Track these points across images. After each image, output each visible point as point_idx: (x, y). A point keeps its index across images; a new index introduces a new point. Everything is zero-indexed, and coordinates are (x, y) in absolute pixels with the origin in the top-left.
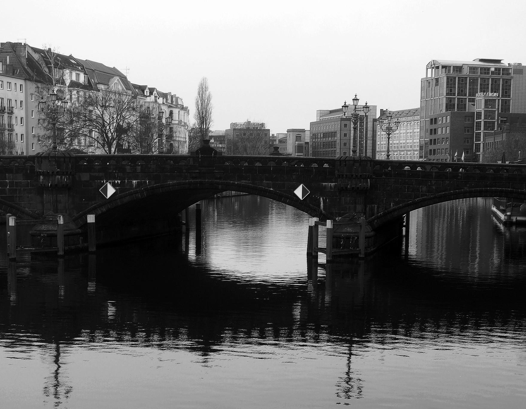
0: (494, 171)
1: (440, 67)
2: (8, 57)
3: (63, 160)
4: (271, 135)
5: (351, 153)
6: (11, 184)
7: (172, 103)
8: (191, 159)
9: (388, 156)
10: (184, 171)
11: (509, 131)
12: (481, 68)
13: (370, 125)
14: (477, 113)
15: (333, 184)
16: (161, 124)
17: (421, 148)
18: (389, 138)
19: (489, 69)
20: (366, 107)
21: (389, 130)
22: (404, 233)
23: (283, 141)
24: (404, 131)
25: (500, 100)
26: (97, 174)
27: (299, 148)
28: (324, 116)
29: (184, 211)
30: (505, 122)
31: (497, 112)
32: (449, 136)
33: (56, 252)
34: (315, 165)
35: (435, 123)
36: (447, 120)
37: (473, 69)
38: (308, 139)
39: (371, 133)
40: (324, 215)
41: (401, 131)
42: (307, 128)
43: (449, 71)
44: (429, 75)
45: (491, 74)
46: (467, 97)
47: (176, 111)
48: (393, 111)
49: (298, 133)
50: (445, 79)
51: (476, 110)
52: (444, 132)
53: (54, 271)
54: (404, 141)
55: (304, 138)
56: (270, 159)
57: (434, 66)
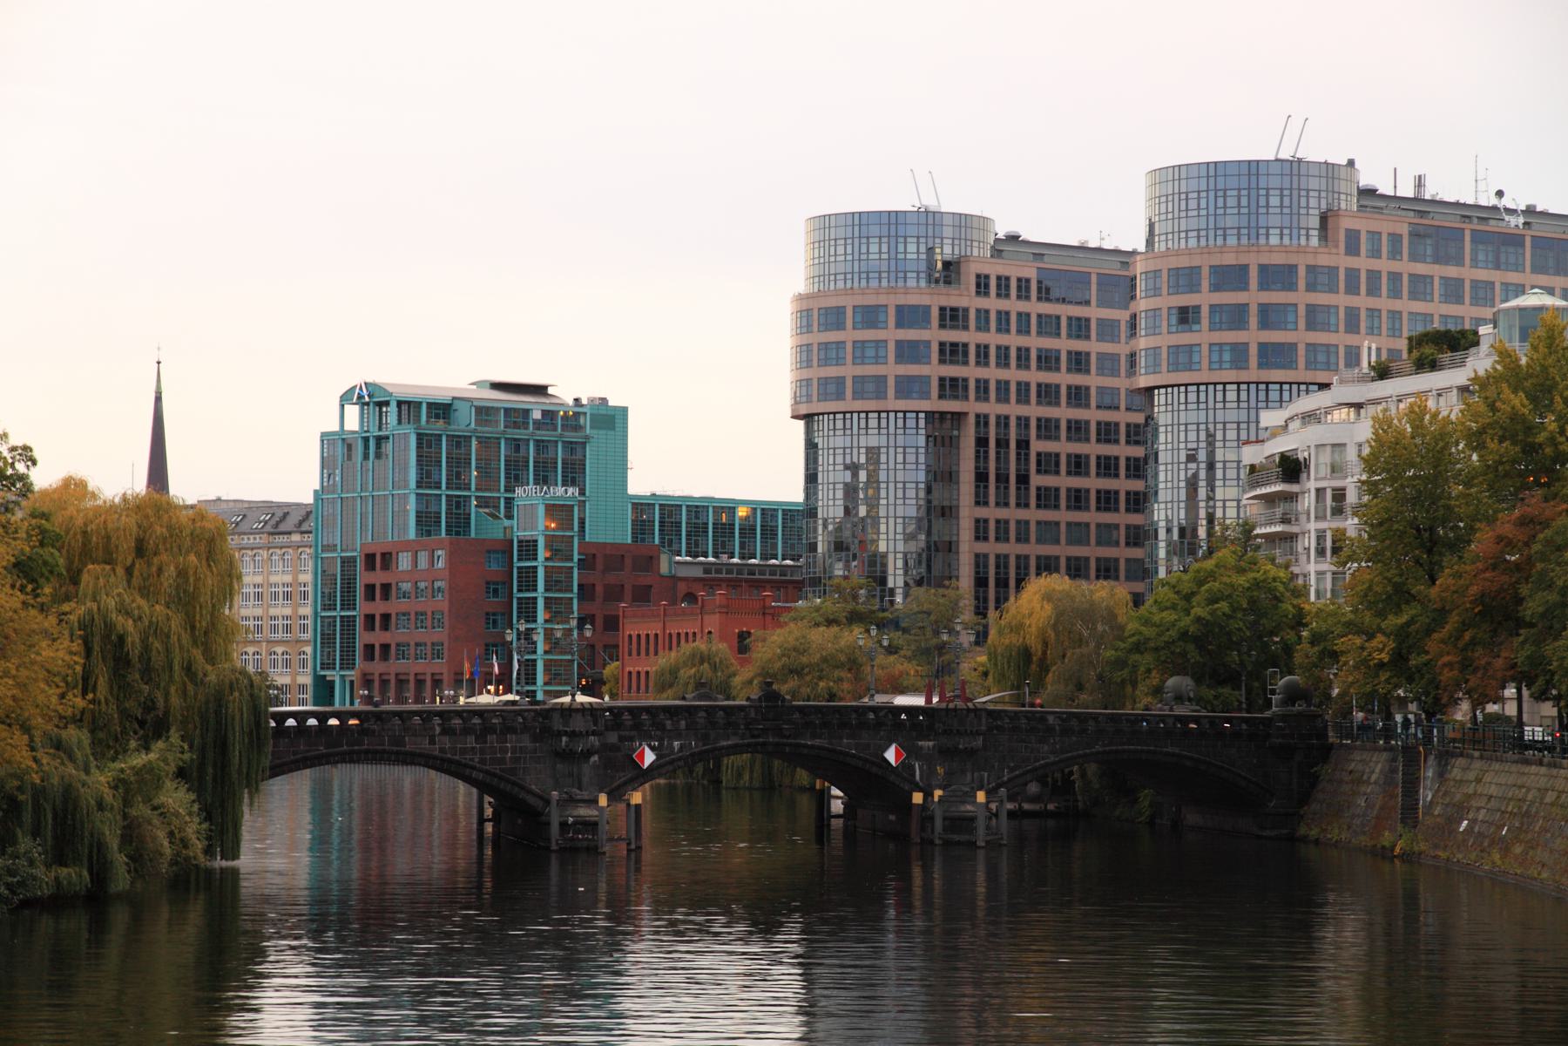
6: (514, 750)
8: (752, 710)
10: (742, 727)
11: (725, 610)
12: (507, 410)
14: (519, 542)
15: (931, 744)
19: (527, 412)
36: (416, 562)
37: (484, 412)
45: (506, 427)
57: (372, 399)
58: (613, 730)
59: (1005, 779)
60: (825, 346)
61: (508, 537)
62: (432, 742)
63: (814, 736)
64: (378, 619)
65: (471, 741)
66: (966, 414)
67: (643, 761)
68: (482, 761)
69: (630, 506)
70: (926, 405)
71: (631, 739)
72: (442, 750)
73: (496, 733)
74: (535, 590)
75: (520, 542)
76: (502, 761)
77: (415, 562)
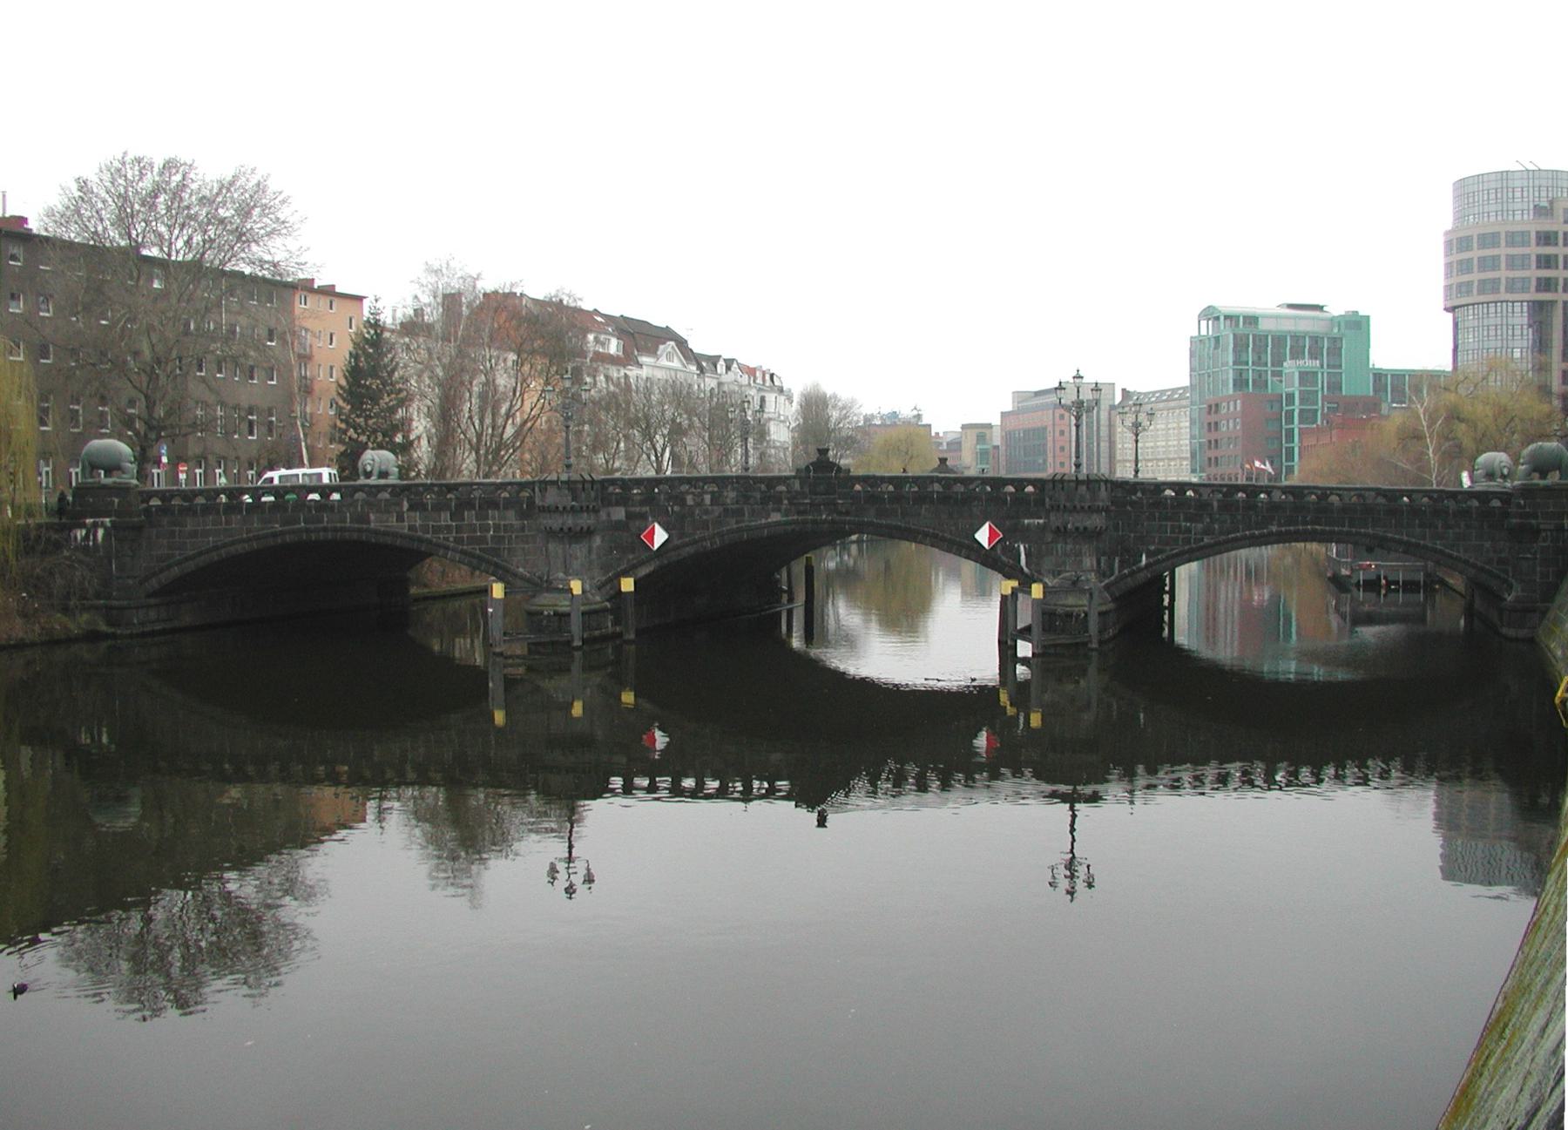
0: (1317, 497)
1: (1222, 318)
3: (580, 486)
4: (933, 434)
5: (1074, 468)
6: (497, 528)
7: (764, 385)
9: (1137, 471)
10: (786, 502)
13: (1104, 416)
16: (745, 422)
17: (1193, 455)
18: (1137, 441)
20: (1097, 388)
21: (1137, 428)
22: (1166, 603)
23: (956, 445)
24: (1163, 426)
25: (1325, 374)
27: (983, 455)
28: (1023, 401)
29: (798, 567)
30: (1336, 410)
31: (1320, 393)
32: (1240, 434)
33: (569, 643)
34: (1011, 489)
35: (1217, 411)
38: (997, 441)
40: (1026, 575)
41: (1158, 427)
42: (996, 421)
43: (1237, 325)
44: (1204, 332)
46: (1269, 368)
47: (770, 398)
48: (1139, 390)
49: (980, 431)
50: (1231, 336)
51: (1285, 389)
52: (1230, 427)
53: (564, 670)
54: (1164, 443)
55: (991, 440)
56: (932, 480)
57: (1210, 314)
60: (1460, 262)
61: (1279, 392)
62: (400, 518)
64: (1213, 425)
65: (445, 518)
66: (1556, 301)
67: (652, 542)
68: (458, 541)
69: (1371, 375)
70: (1527, 297)
72: (411, 528)
73: (474, 509)
74: (1293, 423)
75: (1287, 395)
76: (483, 540)
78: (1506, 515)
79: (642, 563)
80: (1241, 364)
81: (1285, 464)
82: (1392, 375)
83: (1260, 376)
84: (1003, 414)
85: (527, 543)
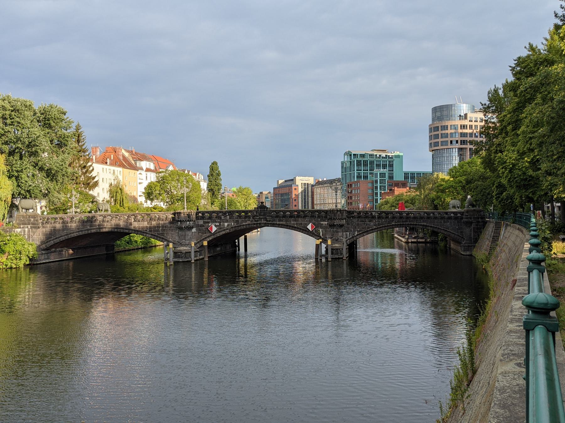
2: (112, 156)
8: (255, 212)
9: (336, 206)
10: (251, 218)
26: (207, 221)
29: (242, 239)
39: (311, 193)
44: (346, 160)
57: (349, 154)
58: (201, 219)
59: (356, 235)
63: (280, 221)
66: (467, 148)
67: (212, 231)
71: (208, 223)
77: (355, 192)
78: (462, 218)
79: (209, 237)
80: (359, 170)
81: (375, 204)
82: (423, 174)
83: (359, 174)
84: (274, 189)
85: (172, 231)
